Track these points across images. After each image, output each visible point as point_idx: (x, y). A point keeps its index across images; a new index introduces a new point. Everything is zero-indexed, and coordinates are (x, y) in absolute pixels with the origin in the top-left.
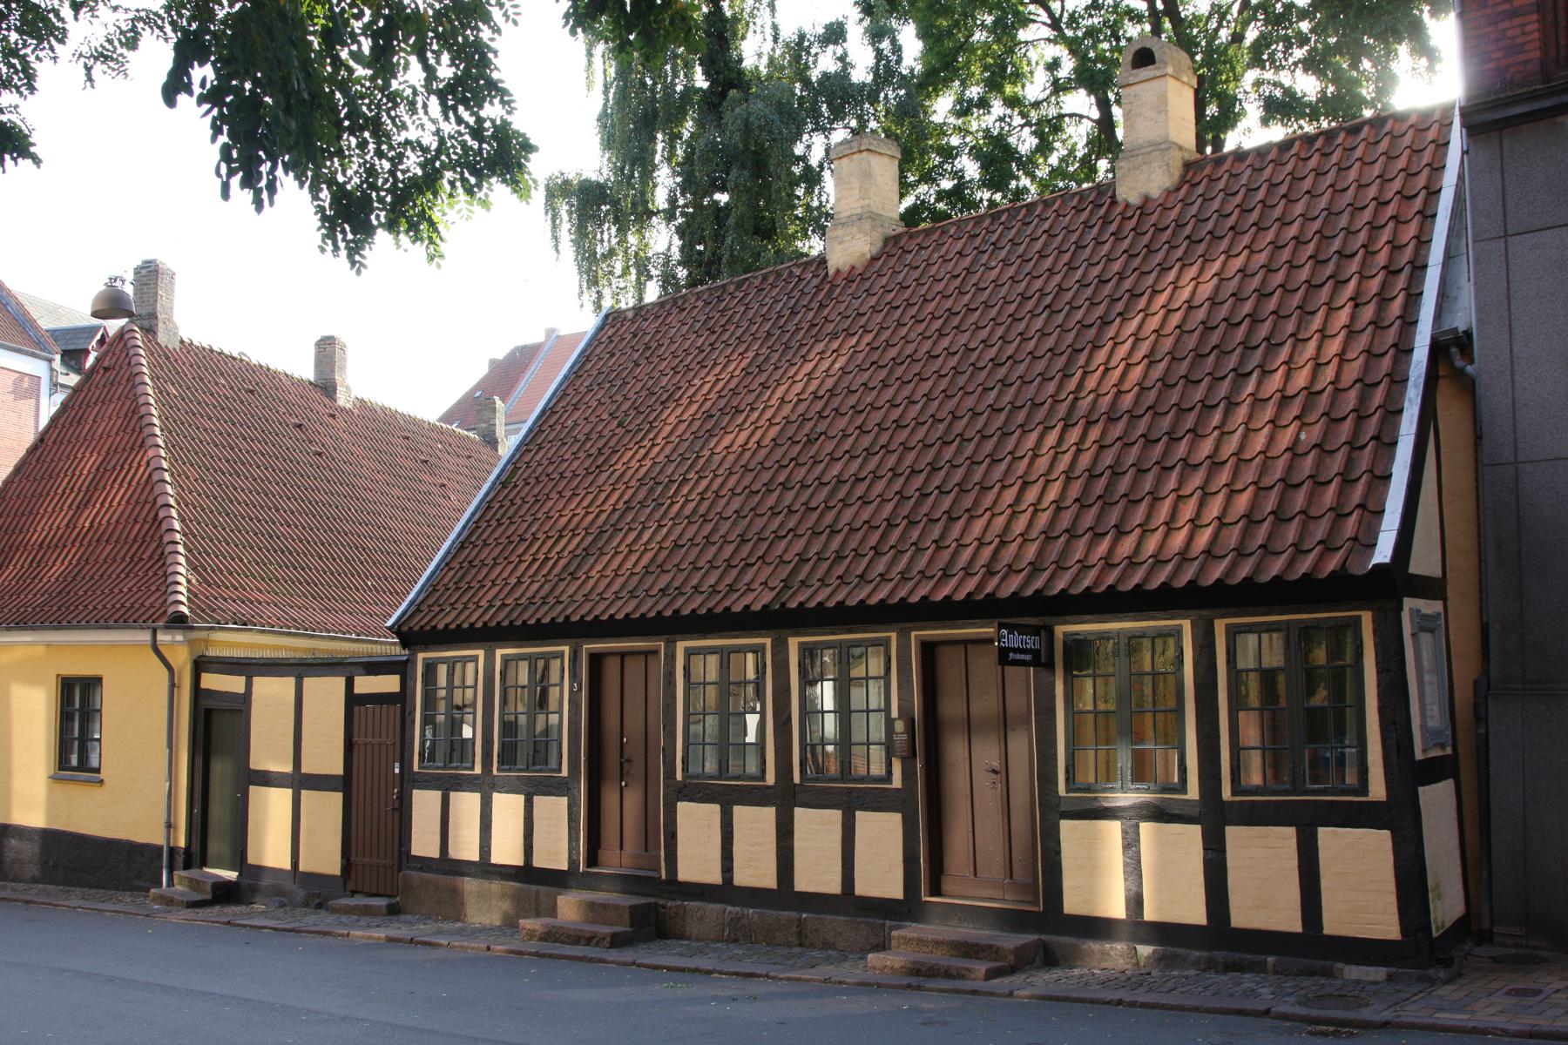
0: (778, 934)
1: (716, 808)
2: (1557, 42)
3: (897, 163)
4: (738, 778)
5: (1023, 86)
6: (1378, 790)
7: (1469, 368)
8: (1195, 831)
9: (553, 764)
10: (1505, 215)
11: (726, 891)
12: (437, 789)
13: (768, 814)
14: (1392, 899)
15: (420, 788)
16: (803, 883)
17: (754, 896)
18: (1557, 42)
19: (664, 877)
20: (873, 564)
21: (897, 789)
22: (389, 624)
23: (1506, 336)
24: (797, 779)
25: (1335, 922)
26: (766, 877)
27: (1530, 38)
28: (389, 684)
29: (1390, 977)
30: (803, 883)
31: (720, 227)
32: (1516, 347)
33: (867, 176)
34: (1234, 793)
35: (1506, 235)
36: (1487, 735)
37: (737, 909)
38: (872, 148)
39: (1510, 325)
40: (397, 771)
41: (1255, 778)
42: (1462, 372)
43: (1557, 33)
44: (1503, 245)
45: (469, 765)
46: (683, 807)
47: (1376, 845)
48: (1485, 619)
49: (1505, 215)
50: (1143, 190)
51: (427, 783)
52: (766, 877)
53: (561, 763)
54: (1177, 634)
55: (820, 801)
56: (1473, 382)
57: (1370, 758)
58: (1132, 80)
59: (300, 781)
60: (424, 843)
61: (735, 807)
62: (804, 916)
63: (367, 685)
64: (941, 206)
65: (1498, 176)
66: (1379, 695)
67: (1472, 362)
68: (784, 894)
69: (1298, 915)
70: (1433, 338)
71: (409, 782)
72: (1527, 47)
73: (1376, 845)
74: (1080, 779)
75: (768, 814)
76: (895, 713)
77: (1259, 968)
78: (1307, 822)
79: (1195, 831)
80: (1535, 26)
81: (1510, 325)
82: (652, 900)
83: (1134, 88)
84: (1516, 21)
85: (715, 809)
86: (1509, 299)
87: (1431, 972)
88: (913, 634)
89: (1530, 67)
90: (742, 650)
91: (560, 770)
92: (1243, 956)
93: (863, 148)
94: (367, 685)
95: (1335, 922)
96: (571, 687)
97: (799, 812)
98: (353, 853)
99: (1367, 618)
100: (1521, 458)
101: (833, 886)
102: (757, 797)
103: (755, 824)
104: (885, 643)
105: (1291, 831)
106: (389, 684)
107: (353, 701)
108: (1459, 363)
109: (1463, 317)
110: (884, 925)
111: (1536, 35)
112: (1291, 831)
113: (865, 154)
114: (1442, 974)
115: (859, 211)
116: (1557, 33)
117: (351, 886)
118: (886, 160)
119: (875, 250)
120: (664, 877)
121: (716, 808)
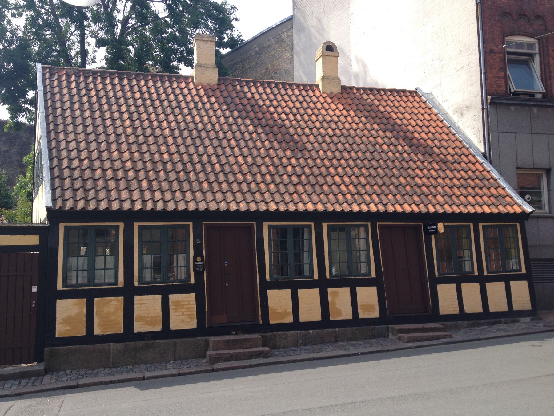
1: (289, 291)
4: (101, 285)
5: (232, 27)
24: (328, 276)
29: (531, 320)
31: (26, 28)
35: (498, 132)
45: (113, 281)
46: (270, 293)
54: (117, 228)
57: (521, 262)
65: (496, 116)
69: (507, 306)
74: (69, 282)
75: (315, 292)
77: (500, 323)
84: (499, 79)
88: (203, 223)
90: (359, 226)
91: (520, 270)
95: (516, 307)
99: (518, 225)
102: (471, 280)
104: (366, 226)
110: (388, 328)
121: (289, 291)
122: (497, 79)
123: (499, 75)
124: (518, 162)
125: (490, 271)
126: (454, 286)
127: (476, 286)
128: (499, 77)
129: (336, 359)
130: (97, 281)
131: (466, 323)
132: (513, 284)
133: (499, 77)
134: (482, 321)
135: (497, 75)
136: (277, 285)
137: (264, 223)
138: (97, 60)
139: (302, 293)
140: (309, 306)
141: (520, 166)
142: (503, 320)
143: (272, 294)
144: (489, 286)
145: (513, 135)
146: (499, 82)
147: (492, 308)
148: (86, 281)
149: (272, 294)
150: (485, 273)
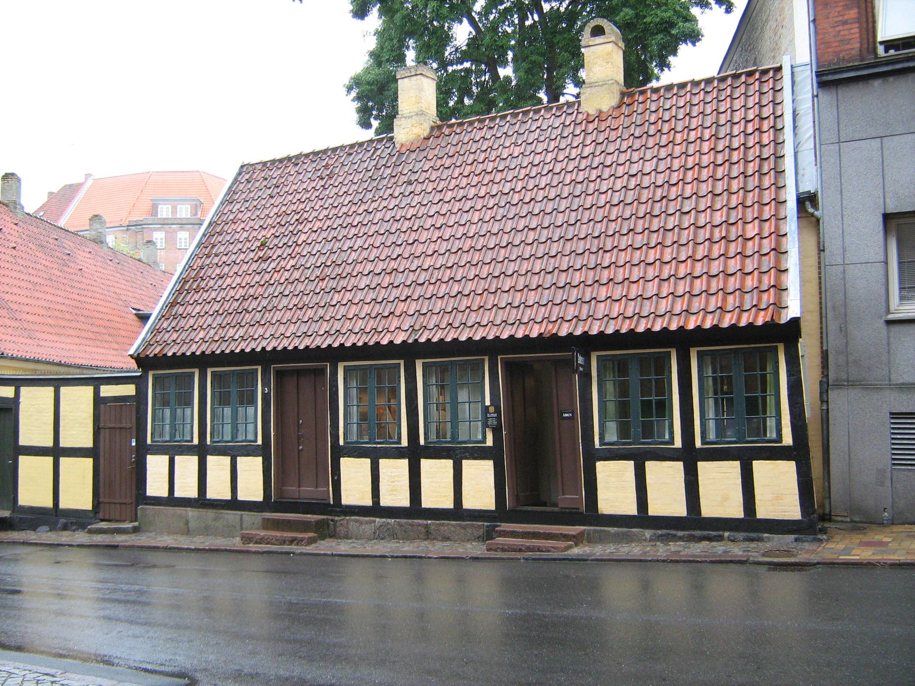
0: (411, 534)
2: (868, 39)
3: (435, 82)
4: (242, 442)
6: (788, 439)
7: (816, 213)
8: (680, 465)
9: (771, 434)
10: (839, 131)
11: (376, 510)
12: (166, 454)
13: (403, 464)
14: (797, 497)
15: (151, 454)
16: (428, 502)
17: (185, 502)
18: (868, 39)
19: (332, 503)
20: (612, 309)
21: (788, 447)
22: (131, 352)
23: (839, 196)
24: (422, 442)
25: (763, 512)
26: (403, 500)
27: (854, 36)
28: (129, 390)
29: (796, 540)
30: (428, 502)
32: (844, 202)
33: (421, 89)
34: (702, 444)
36: (828, 409)
37: (383, 520)
38: (424, 73)
39: (841, 190)
40: (134, 444)
41: (712, 436)
42: (812, 215)
43: (868, 34)
44: (837, 147)
45: (189, 439)
47: (788, 469)
48: (825, 348)
49: (839, 131)
50: (598, 107)
51: (158, 450)
52: (403, 500)
53: (256, 437)
55: (220, 451)
56: (818, 220)
58: (591, 43)
59: (56, 452)
60: (156, 486)
61: (754, 462)
62: (429, 522)
63: (107, 391)
64: (375, 124)
65: (835, 108)
66: (788, 388)
67: (817, 209)
68: (202, 502)
70: (797, 196)
71: (143, 451)
72: (852, 42)
73: (788, 469)
75: (403, 464)
76: (488, 403)
78: (746, 458)
79: (680, 465)
80: (857, 30)
81: (841, 190)
82: (325, 517)
83: (592, 48)
84: (846, 27)
85: (367, 462)
86: (841, 176)
87: (819, 536)
89: (854, 52)
92: (709, 533)
93: (418, 73)
94: (107, 391)
96: (263, 390)
97: (424, 462)
98: (101, 495)
100: (847, 262)
101: (165, 493)
102: (187, 450)
103: (187, 465)
105: (737, 464)
106: (129, 390)
107: (98, 401)
108: (811, 210)
109: (809, 185)
111: (857, 35)
112: (737, 464)
113: (419, 77)
114: (825, 537)
115: (416, 110)
116: (868, 34)
117: (101, 516)
118: (430, 81)
119: (426, 133)
120: (332, 503)
122: (841, 28)
123: (846, 17)
124: (888, 200)
125: (606, 441)
126: (367, 462)
127: (677, 468)
128: (845, 23)
129: (365, 559)
130: (460, 439)
131: (648, 533)
132: (759, 467)
133: (845, 23)
134: (680, 533)
135: (841, 18)
136: (356, 452)
137: (339, 364)
138: (16, 222)
139: (385, 464)
140: (393, 484)
141: (891, 209)
142: (726, 534)
143: (603, 468)
144: (211, 460)
145: (876, 143)
146: (846, 32)
147: (708, 510)
148: (229, 439)
149: (603, 468)
150: (698, 444)
